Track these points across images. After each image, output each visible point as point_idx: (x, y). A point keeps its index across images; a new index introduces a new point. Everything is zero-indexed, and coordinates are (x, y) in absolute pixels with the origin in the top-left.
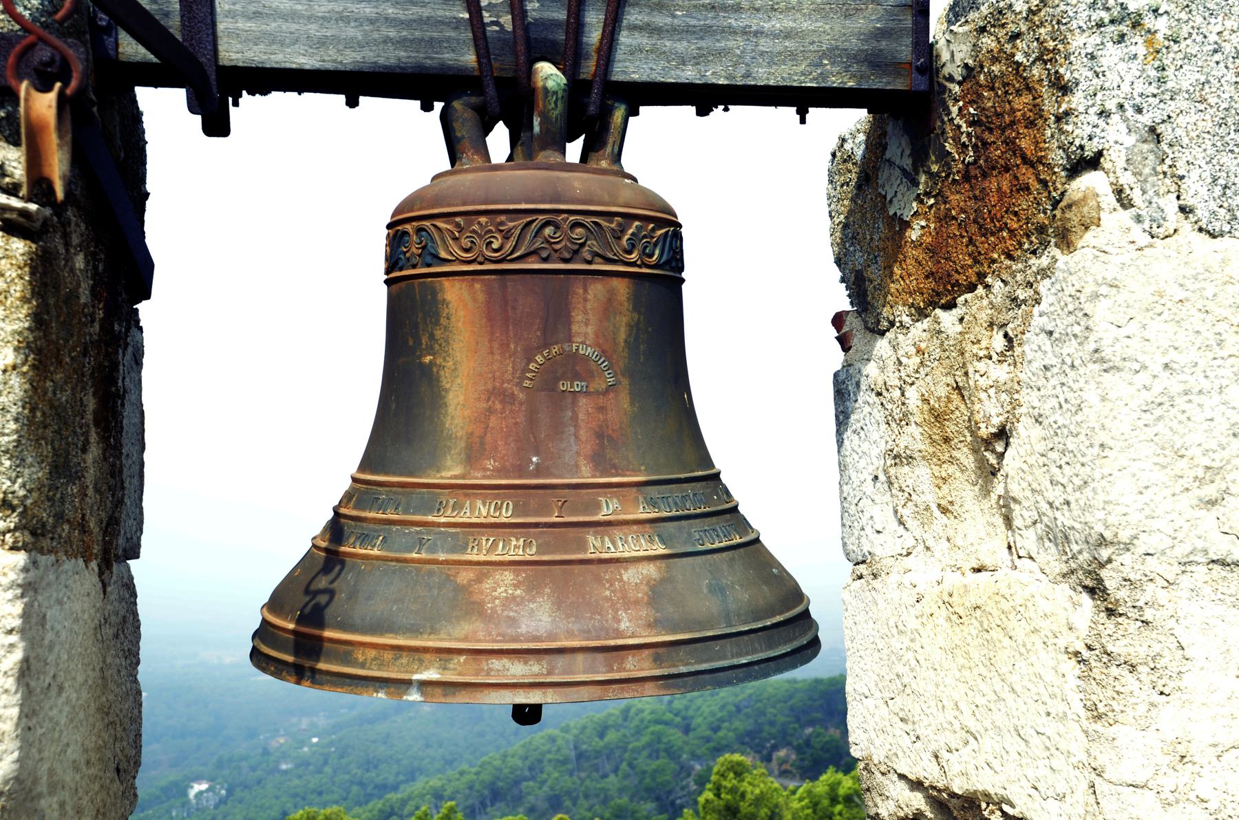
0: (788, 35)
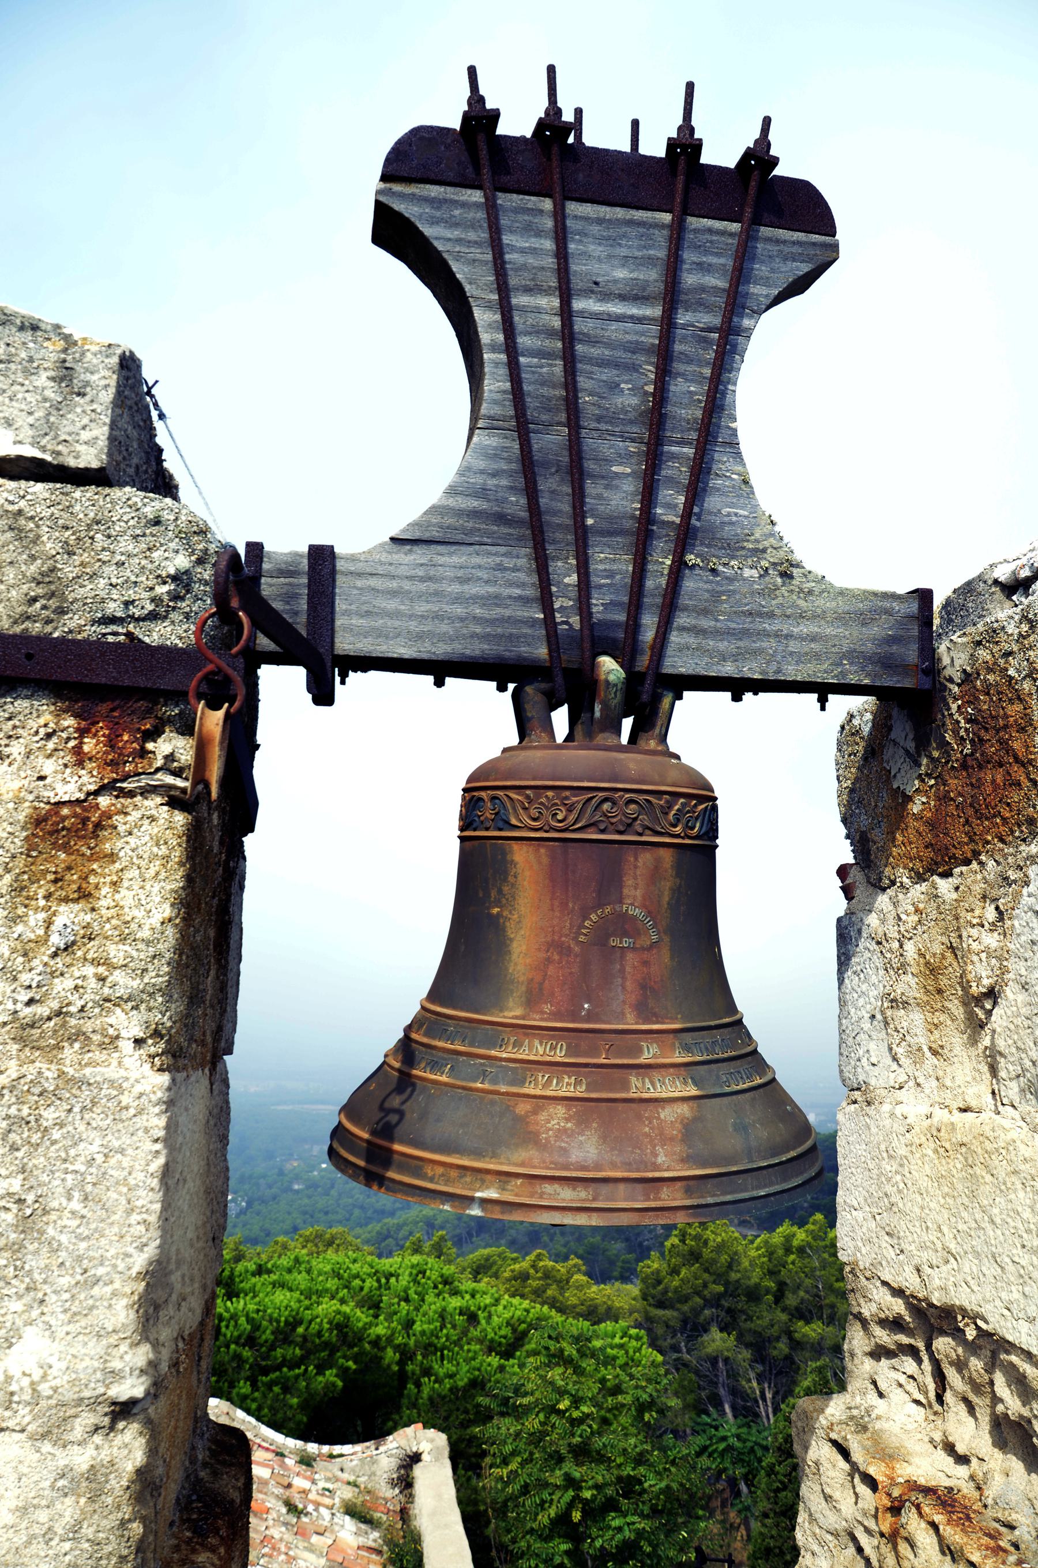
0: (813, 638)
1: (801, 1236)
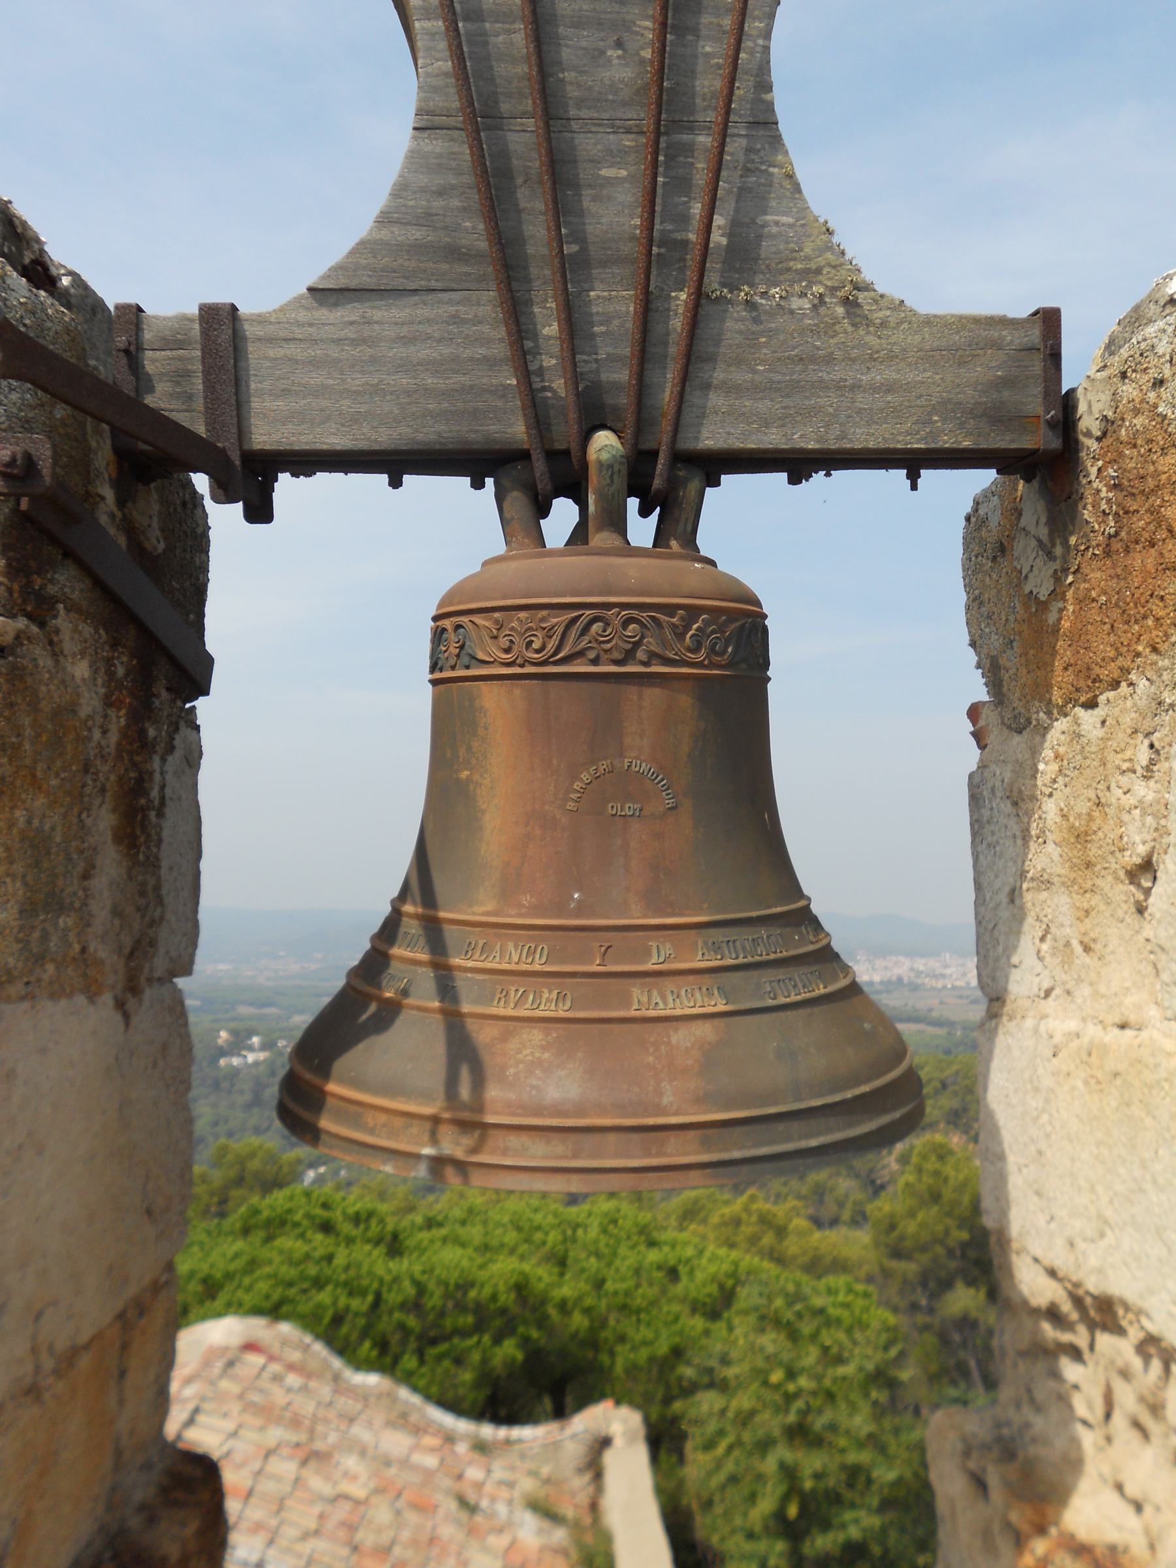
0: (890, 388)
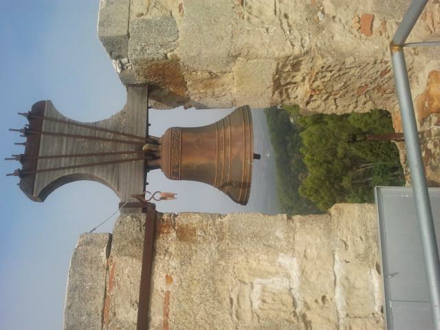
1: (308, 156)
